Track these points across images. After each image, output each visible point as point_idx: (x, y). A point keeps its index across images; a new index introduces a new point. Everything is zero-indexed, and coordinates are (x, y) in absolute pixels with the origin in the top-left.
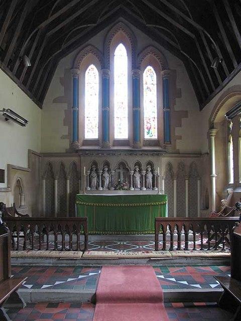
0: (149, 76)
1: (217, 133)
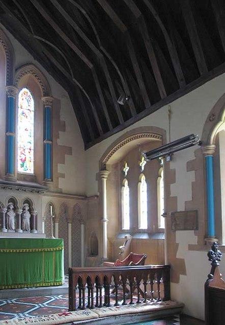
0: (25, 101)
1: (109, 175)
